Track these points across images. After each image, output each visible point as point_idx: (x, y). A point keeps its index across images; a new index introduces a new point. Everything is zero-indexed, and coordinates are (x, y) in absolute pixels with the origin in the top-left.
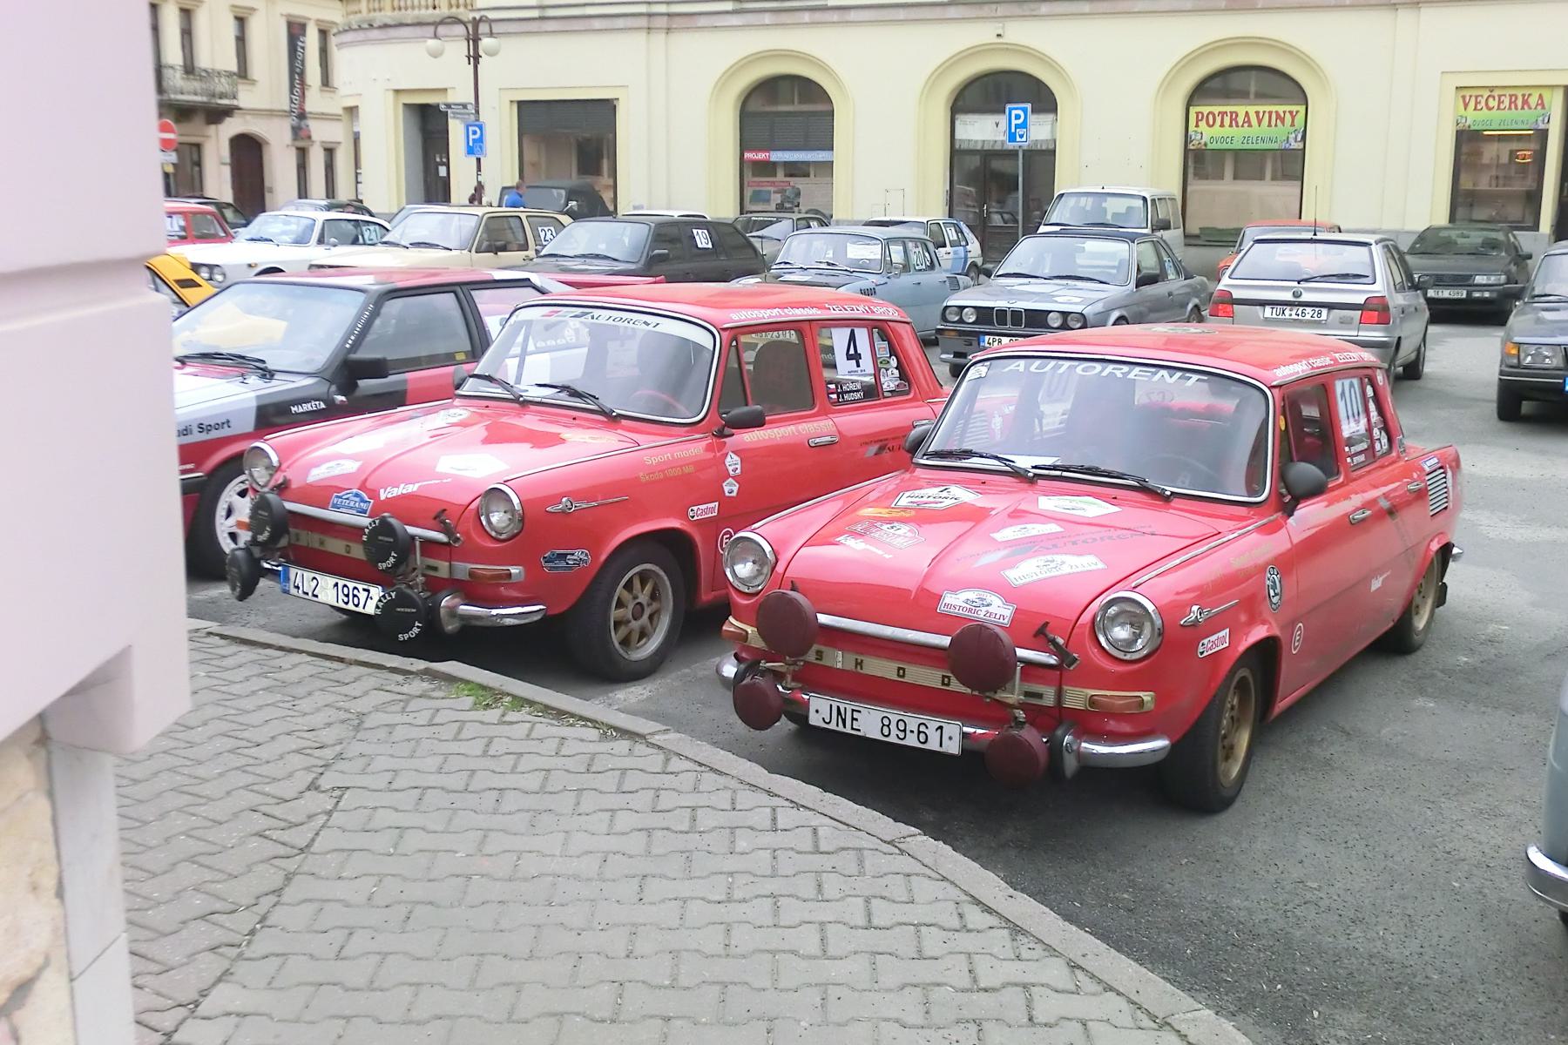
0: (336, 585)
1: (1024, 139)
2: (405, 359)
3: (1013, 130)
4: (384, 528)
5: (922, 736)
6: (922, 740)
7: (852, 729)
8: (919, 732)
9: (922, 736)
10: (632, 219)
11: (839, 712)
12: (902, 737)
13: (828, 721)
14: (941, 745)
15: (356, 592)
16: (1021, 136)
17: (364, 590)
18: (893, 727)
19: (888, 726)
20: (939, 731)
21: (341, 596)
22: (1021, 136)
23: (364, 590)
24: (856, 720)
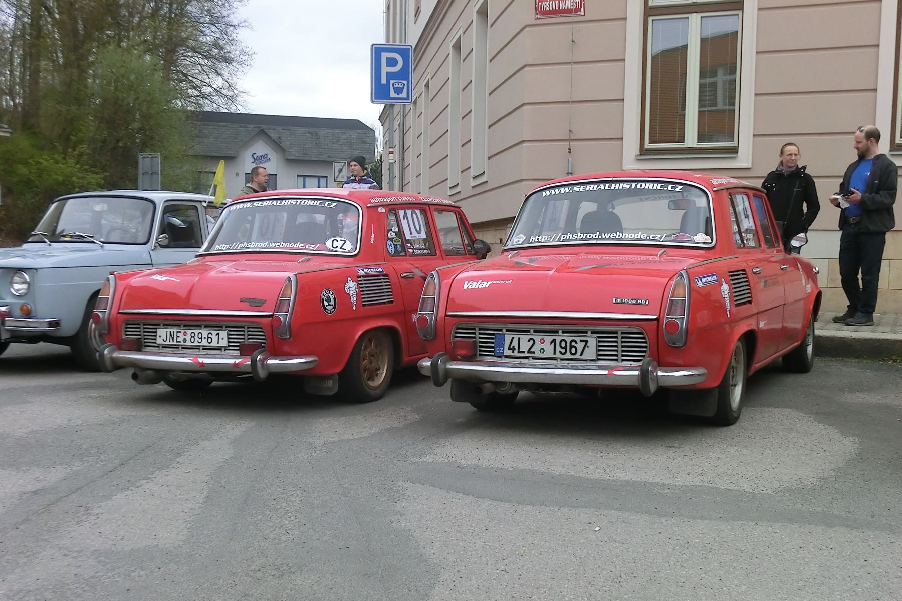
0: (554, 341)
1: (404, 95)
2: (891, 144)
3: (384, 81)
4: (64, 158)
5: (210, 339)
6: (210, 341)
7: (177, 342)
8: (201, 338)
9: (210, 339)
10: (869, 160)
11: (171, 335)
12: (200, 341)
13: (165, 340)
14: (218, 343)
15: (573, 344)
16: (399, 91)
17: (581, 341)
18: (196, 337)
19: (194, 337)
20: (218, 335)
21: (558, 349)
22: (399, 91)
23: (581, 341)
24: (179, 336)
